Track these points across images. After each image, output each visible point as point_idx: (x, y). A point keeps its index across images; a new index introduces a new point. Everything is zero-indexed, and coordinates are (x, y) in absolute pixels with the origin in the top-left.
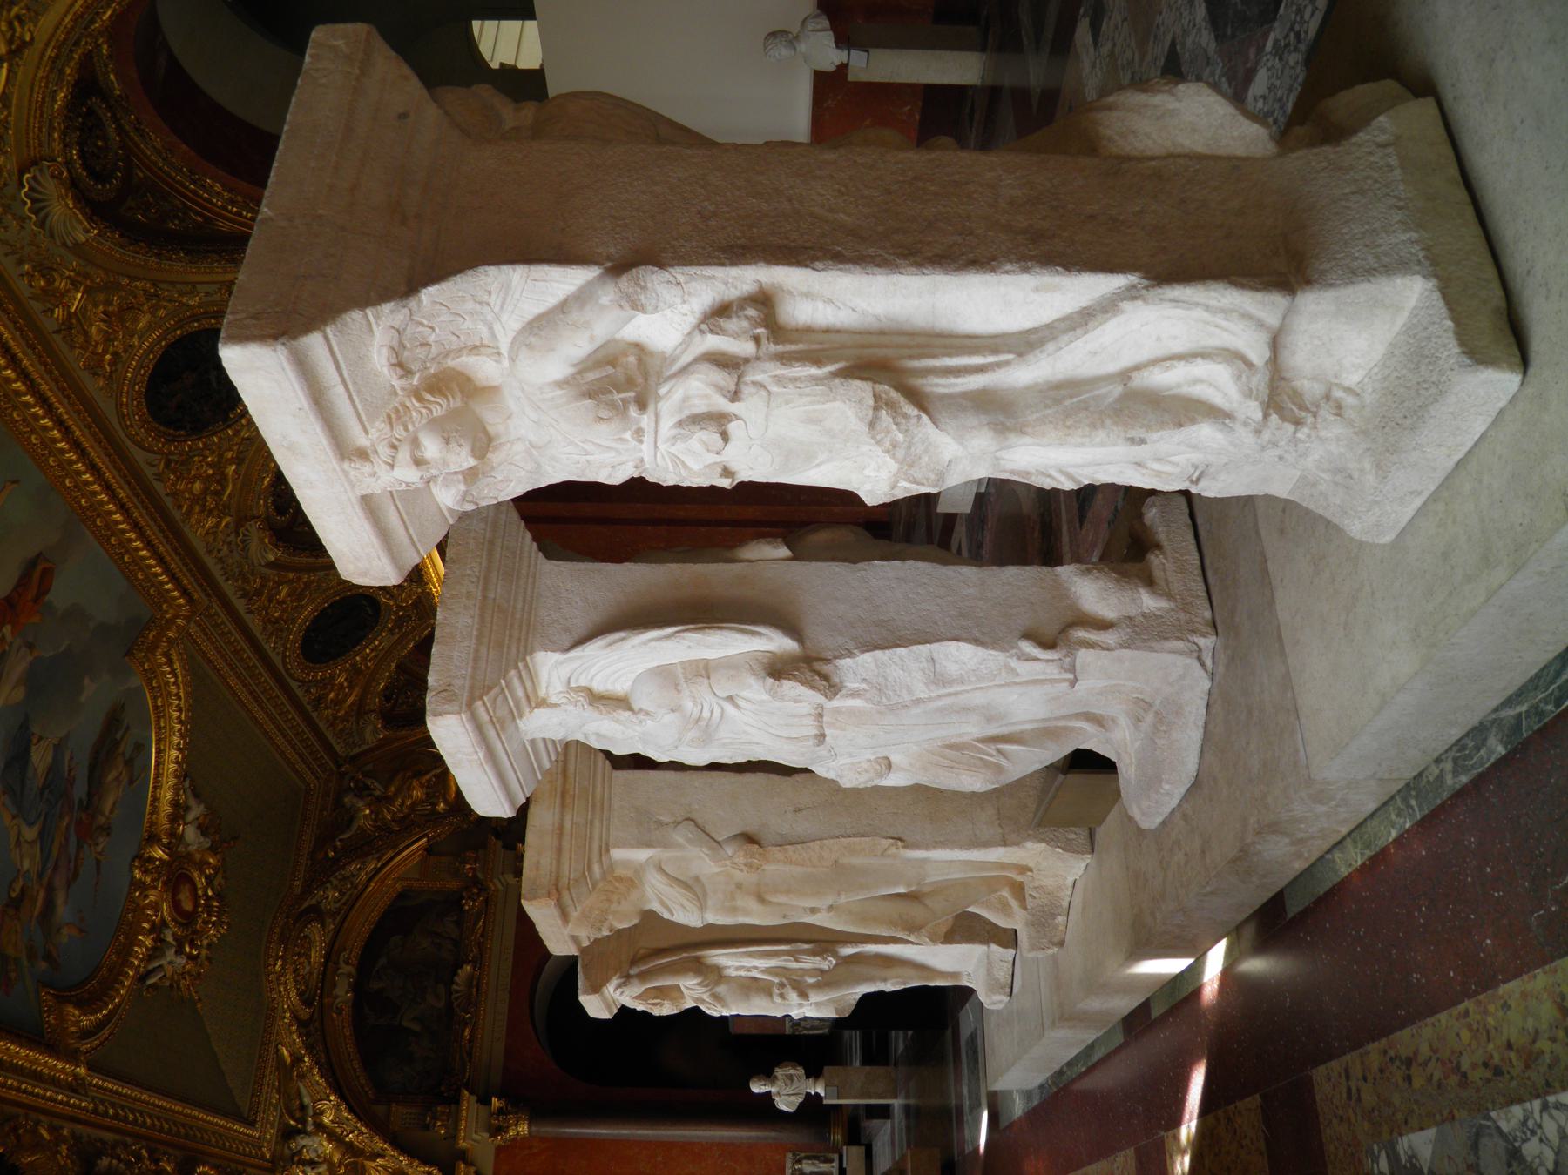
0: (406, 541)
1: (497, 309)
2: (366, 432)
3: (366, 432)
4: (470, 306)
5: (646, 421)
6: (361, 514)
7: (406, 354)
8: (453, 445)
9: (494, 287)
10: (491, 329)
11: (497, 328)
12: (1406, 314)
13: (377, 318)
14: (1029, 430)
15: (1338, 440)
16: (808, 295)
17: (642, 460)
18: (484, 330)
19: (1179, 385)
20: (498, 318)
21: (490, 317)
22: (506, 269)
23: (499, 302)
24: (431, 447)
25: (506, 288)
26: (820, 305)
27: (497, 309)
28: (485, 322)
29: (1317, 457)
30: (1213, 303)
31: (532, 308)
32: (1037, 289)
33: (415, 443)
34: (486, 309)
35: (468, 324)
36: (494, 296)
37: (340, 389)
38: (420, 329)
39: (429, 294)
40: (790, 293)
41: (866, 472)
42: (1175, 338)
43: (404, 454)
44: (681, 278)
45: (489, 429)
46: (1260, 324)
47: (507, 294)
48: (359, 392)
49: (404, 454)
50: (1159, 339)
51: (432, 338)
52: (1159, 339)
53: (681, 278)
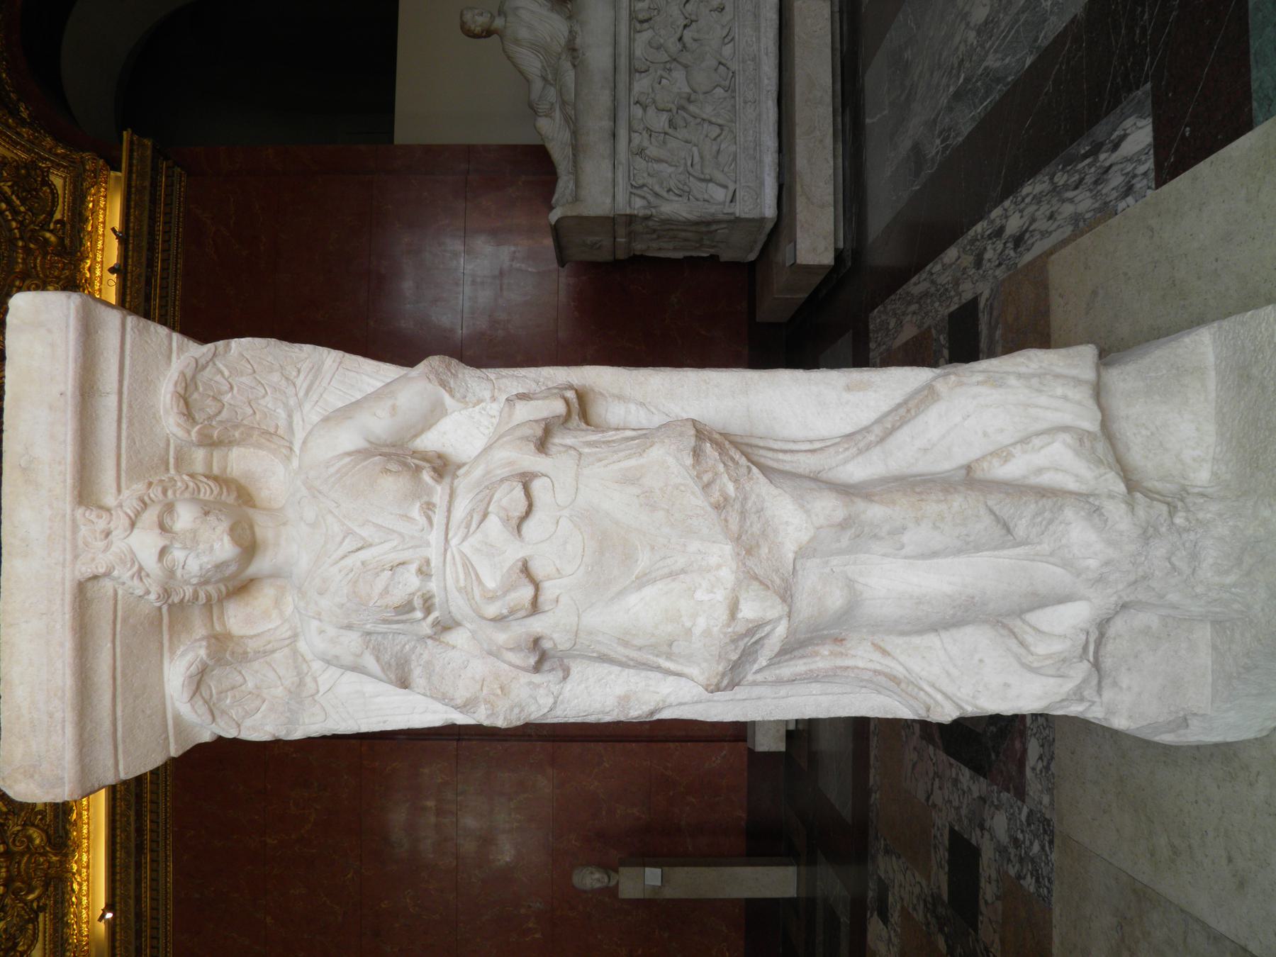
0: (107, 724)
1: (301, 394)
2: (119, 490)
3: (119, 490)
4: (275, 377)
5: (439, 493)
6: (68, 598)
7: (196, 396)
8: (211, 518)
9: (305, 366)
10: (290, 416)
11: (297, 418)
12: (1213, 373)
13: (180, 349)
14: (876, 498)
15: (1220, 515)
16: (620, 398)
17: (428, 562)
18: (282, 413)
19: (1024, 477)
20: (300, 405)
21: (292, 402)
22: (323, 351)
23: (305, 385)
24: (185, 517)
25: (317, 371)
26: (633, 407)
27: (301, 394)
28: (286, 405)
29: (1211, 561)
30: (1023, 370)
31: (335, 400)
32: (848, 388)
33: (169, 508)
34: (290, 391)
35: (268, 402)
36: (302, 376)
37: (112, 401)
38: (218, 378)
39: (240, 347)
40: (601, 394)
41: (700, 595)
42: (1002, 431)
43: (151, 516)
44: (492, 377)
45: (257, 529)
46: (1078, 381)
47: (315, 377)
48: (131, 423)
49: (151, 516)
50: (985, 434)
51: (227, 398)
52: (985, 434)
53: (492, 377)
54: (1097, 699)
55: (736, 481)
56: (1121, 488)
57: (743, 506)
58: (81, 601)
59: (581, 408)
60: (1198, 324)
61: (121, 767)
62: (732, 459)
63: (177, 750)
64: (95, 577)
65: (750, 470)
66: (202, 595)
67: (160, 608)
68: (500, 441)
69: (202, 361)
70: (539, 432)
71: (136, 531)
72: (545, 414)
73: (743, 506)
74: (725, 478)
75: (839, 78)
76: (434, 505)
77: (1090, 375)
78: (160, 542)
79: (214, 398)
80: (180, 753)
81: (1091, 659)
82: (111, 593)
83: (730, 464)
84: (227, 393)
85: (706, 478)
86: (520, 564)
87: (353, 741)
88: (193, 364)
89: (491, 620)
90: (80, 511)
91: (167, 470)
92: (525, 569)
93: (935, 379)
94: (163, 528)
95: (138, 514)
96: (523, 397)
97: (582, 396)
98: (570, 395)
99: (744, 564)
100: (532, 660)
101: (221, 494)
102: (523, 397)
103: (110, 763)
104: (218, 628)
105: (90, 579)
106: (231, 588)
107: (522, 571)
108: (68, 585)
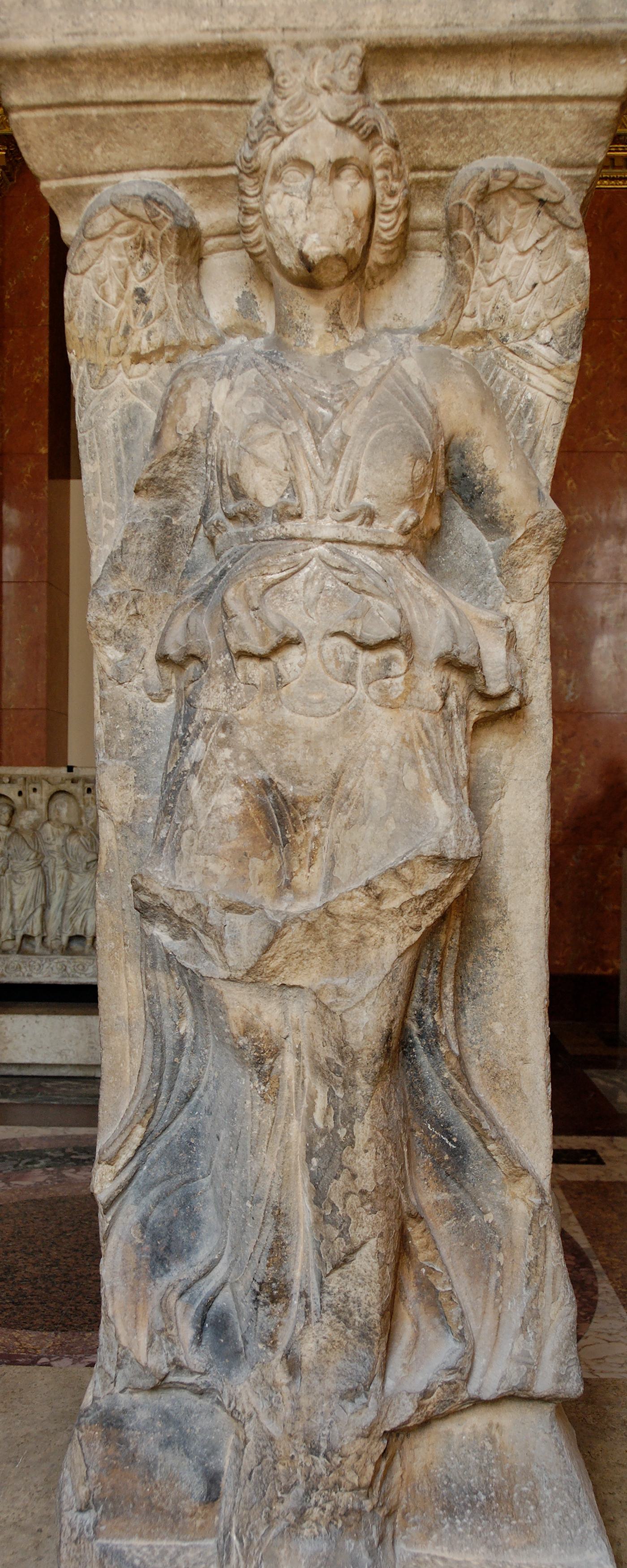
7: (513, 203)
13: (577, 180)
54: (120, 1385)
55: (401, 909)
56: (394, 1422)
57: (369, 920)
58: (240, 55)
59: (501, 713)
60: (571, 1419)
61: (25, 114)
62: (431, 905)
63: (48, 190)
64: (271, 73)
65: (417, 928)
66: (251, 220)
67: (232, 164)
68: (453, 614)
69: (558, 211)
70: (464, 659)
71: (332, 128)
72: (488, 669)
73: (369, 920)
74: (404, 897)
75: (79, 1073)
76: (370, 524)
77: (544, 1385)
78: (319, 162)
79: (509, 230)
80: (46, 195)
81: (171, 1379)
82: (252, 96)
83: (424, 903)
84: (516, 246)
85: (406, 872)
86: (294, 634)
87: (41, 374)
88: (555, 198)
89: (223, 599)
90: (358, 49)
91: (414, 169)
92: (289, 642)
93: (535, 1178)
94: (338, 166)
95: (354, 129)
96: (512, 639)
97: (516, 713)
98: (513, 701)
99: (294, 921)
100: (172, 651)
101: (384, 243)
102: (512, 639)
103: (32, 100)
104: (210, 244)
105: (269, 65)
106: (261, 258)
107: (285, 638)
108: (263, 36)
